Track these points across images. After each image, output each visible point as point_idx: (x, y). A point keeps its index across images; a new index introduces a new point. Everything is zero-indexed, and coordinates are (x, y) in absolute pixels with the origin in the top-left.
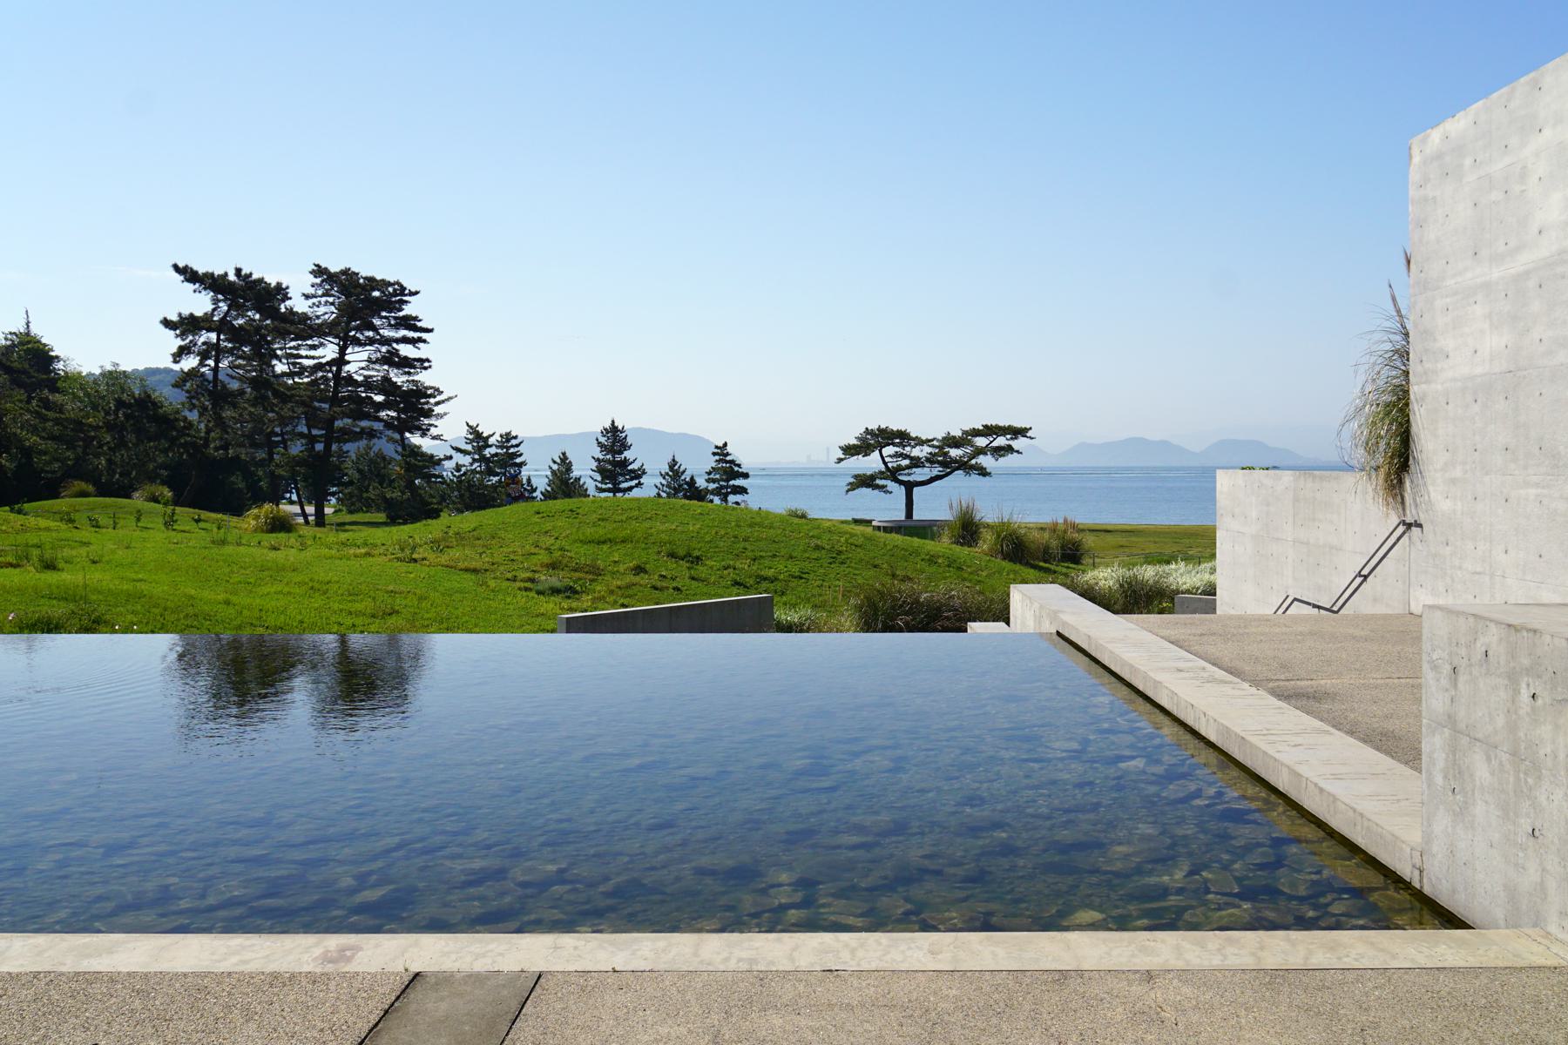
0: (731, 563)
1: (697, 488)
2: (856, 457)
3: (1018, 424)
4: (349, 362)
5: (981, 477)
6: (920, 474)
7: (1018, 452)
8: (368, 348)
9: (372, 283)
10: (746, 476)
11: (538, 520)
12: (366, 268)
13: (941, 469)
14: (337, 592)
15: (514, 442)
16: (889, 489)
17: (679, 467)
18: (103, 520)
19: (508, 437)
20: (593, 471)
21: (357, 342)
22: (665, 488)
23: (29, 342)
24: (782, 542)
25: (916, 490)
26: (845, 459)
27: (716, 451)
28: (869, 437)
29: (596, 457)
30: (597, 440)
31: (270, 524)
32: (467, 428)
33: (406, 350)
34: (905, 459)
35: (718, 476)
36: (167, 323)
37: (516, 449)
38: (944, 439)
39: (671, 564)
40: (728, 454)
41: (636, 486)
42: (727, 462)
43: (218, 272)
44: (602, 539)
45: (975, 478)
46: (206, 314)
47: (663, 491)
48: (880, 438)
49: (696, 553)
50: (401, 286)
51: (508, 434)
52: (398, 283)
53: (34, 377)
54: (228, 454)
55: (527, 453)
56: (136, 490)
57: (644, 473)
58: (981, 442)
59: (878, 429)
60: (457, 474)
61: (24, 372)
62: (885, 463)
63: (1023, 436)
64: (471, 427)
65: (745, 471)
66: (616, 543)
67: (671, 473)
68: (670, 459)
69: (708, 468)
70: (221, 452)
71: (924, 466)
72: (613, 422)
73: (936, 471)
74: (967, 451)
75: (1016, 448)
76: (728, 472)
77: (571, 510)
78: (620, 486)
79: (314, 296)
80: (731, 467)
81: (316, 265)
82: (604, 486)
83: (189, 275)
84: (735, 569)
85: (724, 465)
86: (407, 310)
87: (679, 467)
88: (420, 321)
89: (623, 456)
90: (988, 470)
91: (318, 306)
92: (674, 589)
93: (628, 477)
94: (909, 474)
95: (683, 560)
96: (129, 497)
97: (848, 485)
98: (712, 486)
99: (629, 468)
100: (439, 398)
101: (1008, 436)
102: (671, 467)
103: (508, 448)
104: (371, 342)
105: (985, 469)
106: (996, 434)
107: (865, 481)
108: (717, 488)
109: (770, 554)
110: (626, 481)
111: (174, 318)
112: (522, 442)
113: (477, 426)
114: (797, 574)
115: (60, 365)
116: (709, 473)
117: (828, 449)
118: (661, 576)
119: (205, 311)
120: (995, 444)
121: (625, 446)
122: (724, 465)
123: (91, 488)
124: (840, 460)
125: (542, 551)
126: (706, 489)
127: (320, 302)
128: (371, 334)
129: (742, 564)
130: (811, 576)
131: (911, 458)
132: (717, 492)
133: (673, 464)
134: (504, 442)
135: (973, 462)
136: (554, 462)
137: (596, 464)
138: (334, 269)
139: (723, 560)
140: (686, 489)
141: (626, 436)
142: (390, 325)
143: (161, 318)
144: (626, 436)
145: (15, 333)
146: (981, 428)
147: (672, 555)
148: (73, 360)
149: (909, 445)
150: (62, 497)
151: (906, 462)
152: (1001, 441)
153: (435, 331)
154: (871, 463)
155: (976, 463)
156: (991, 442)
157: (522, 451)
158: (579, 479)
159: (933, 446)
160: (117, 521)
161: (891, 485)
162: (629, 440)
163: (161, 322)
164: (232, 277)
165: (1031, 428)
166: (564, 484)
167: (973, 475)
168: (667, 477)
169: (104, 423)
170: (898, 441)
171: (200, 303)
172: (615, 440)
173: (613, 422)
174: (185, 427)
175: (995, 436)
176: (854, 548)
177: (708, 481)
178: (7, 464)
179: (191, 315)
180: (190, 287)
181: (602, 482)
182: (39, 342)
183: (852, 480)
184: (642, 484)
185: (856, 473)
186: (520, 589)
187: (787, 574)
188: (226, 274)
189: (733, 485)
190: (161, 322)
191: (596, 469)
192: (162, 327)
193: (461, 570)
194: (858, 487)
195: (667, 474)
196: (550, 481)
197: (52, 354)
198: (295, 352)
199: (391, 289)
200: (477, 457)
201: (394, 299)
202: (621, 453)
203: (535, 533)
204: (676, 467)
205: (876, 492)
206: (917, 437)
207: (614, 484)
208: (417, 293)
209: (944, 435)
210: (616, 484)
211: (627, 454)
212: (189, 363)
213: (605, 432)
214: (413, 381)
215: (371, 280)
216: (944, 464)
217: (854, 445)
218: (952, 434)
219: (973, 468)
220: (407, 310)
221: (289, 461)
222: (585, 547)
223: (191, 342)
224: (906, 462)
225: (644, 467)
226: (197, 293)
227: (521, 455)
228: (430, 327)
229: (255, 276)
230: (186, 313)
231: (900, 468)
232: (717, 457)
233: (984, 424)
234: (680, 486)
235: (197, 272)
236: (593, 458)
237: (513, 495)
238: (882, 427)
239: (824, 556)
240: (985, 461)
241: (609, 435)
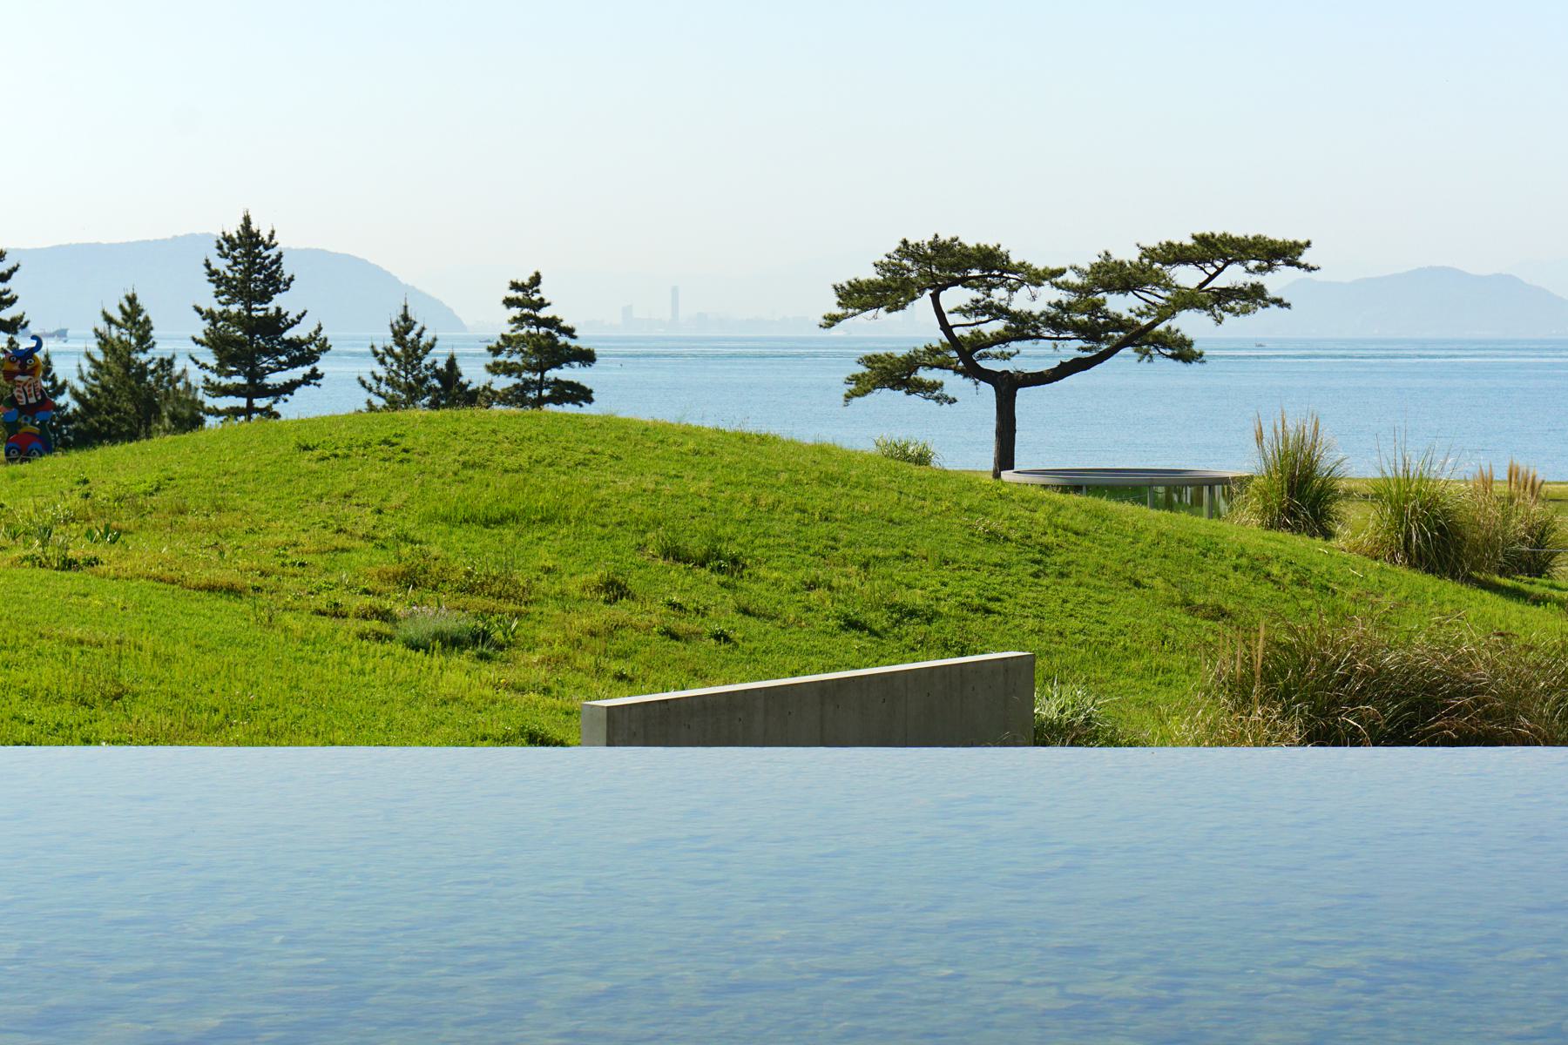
2: (873, 311)
3: (1279, 233)
5: (1180, 363)
6: (1032, 356)
7: (1279, 302)
10: (587, 357)
11: (314, 466)
13: (1080, 343)
14: (210, 618)
16: (948, 391)
17: (419, 335)
20: (197, 342)
22: (384, 388)
26: (844, 317)
27: (513, 294)
28: (907, 263)
29: (205, 308)
30: (208, 265)
34: (997, 318)
35: (517, 359)
38: (1097, 269)
40: (541, 304)
41: (306, 380)
44: (495, 514)
45: (1163, 367)
47: (379, 395)
57: (324, 348)
58: (1187, 276)
62: (946, 328)
63: (1289, 264)
65: (584, 346)
66: (531, 522)
67: (398, 350)
68: (396, 316)
69: (496, 339)
72: (247, 220)
73: (1072, 348)
74: (1152, 299)
75: (1272, 291)
77: (386, 442)
78: (266, 381)
80: (549, 334)
82: (224, 381)
85: (534, 330)
87: (419, 335)
89: (271, 308)
90: (1196, 348)
93: (283, 358)
94: (1006, 357)
95: (703, 565)
97: (849, 381)
98: (502, 383)
99: (287, 335)
101: (1253, 264)
102: (399, 335)
105: (1190, 344)
106: (1224, 256)
108: (516, 386)
109: (896, 552)
110: (280, 367)
112: (15, 269)
114: (977, 601)
116: (496, 351)
117: (675, 291)
118: (672, 605)
120: (1220, 282)
121: (275, 282)
122: (534, 330)
124: (833, 320)
125: (358, 543)
129: (847, 577)
130: (1009, 605)
131: (1012, 316)
135: (1161, 328)
136: (109, 320)
137: (206, 325)
139: (794, 567)
140: (436, 389)
141: (280, 256)
144: (280, 256)
146: (1189, 242)
147: (674, 554)
151: (997, 326)
152: (1235, 276)
155: (1169, 328)
156: (1211, 277)
157: (14, 293)
158: (170, 363)
159: (1066, 287)
161: (952, 382)
162: (287, 269)
165: (1308, 244)
167: (1158, 360)
168: (388, 360)
170: (975, 273)
173: (247, 220)
175: (1219, 264)
176: (1073, 538)
183: (861, 369)
184: (321, 376)
185: (869, 353)
186: (362, 636)
187: (952, 601)
189: (557, 381)
191: (203, 338)
193: (199, 588)
195: (390, 352)
202: (265, 297)
203: (320, 498)
204: (412, 335)
205: (916, 399)
209: (1098, 260)
210: (255, 375)
211: (279, 301)
213: (227, 245)
216: (1089, 332)
217: (871, 282)
218: (1117, 256)
219: (1162, 341)
222: (459, 532)
224: (997, 326)
225: (323, 334)
227: (12, 301)
231: (979, 342)
232: (516, 312)
233: (1197, 233)
236: (199, 310)
237: (23, 402)
239: (1015, 558)
240: (1189, 323)
241: (236, 254)
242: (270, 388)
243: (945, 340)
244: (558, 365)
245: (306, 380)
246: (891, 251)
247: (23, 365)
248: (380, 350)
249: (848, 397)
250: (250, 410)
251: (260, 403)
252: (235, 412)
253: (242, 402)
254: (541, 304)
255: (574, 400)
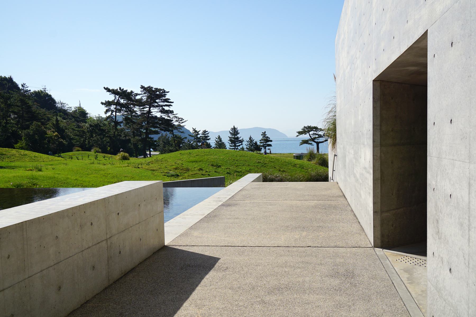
0: (229, 167)
1: (258, 145)
2: (302, 135)
4: (152, 112)
6: (321, 140)
8: (157, 108)
9: (157, 90)
10: (271, 141)
12: (155, 86)
15: (207, 133)
16: (313, 144)
18: (80, 157)
19: (205, 131)
21: (154, 106)
22: (248, 145)
23: (80, 109)
24: (248, 161)
25: (320, 144)
26: (299, 135)
27: (262, 134)
30: (230, 132)
31: (122, 158)
32: (193, 129)
33: (166, 108)
34: (316, 135)
35: (263, 141)
36: (102, 103)
37: (207, 135)
39: (211, 168)
40: (266, 135)
41: (241, 145)
42: (266, 137)
43: (115, 89)
46: (113, 100)
48: (307, 130)
49: (220, 164)
50: (164, 90)
51: (205, 131)
52: (163, 90)
53: (80, 119)
54: (126, 138)
55: (210, 136)
56: (92, 149)
57: (243, 141)
59: (308, 127)
60: (188, 142)
61: (78, 117)
62: (310, 136)
64: (194, 129)
66: (198, 162)
67: (250, 141)
68: (249, 137)
69: (260, 139)
70: (124, 138)
71: (323, 137)
76: (266, 140)
77: (190, 153)
79: (141, 94)
81: (141, 86)
82: (232, 145)
83: (108, 90)
84: (229, 169)
85: (265, 138)
86: (167, 97)
88: (170, 100)
91: (143, 97)
92: (208, 175)
93: (239, 142)
94: (318, 140)
96: (90, 151)
97: (300, 143)
98: (261, 144)
99: (239, 139)
100: (183, 121)
103: (205, 135)
104: (157, 106)
107: (305, 142)
108: (263, 145)
109: (242, 164)
111: (104, 102)
113: (195, 128)
115: (89, 115)
116: (261, 141)
119: (112, 100)
121: (238, 133)
122: (265, 138)
123: (80, 149)
124: (298, 136)
126: (260, 145)
127: (143, 96)
128: (156, 104)
132: (263, 146)
133: (250, 138)
134: (204, 133)
136: (216, 138)
138: (146, 86)
141: (238, 130)
142: (162, 101)
143: (101, 102)
144: (238, 130)
145: (77, 107)
147: (212, 165)
148: (91, 114)
149: (318, 131)
150: (74, 151)
151: (317, 136)
153: (174, 103)
154: (306, 137)
157: (209, 135)
160: (83, 157)
161: (313, 143)
162: (239, 132)
163: (101, 103)
164: (119, 90)
166: (220, 145)
168: (249, 142)
169: (87, 131)
171: (111, 97)
172: (235, 132)
174: (107, 132)
177: (260, 143)
178: (65, 143)
179: (108, 101)
180: (109, 93)
181: (231, 144)
182: (83, 109)
183: (301, 142)
185: (302, 139)
187: (245, 170)
188: (117, 89)
189: (268, 144)
190: (101, 103)
192: (101, 105)
194: (303, 144)
196: (216, 144)
197: (86, 112)
198: (143, 110)
199: (162, 91)
200: (195, 137)
201: (163, 94)
202: (236, 135)
204: (251, 139)
206: (320, 128)
207: (235, 144)
208: (169, 92)
211: (238, 136)
212: (109, 114)
214: (176, 116)
215: (156, 89)
220: (167, 97)
221: (136, 140)
223: (109, 108)
226: (110, 95)
227: (209, 136)
228: (173, 102)
229: (124, 90)
230: (107, 100)
231: (315, 138)
232: (263, 136)
234: (253, 144)
235: (110, 89)
236: (229, 137)
238: (309, 126)
241: (233, 130)
242: (61, 152)
243: (311, 138)
244: (268, 142)
245: (241, 145)
246: (303, 127)
247: (203, 144)
248: (248, 141)
249: (300, 145)
250: (235, 148)
251: (236, 147)
252: (233, 149)
253: (234, 147)
254: (266, 135)
255: (270, 146)
